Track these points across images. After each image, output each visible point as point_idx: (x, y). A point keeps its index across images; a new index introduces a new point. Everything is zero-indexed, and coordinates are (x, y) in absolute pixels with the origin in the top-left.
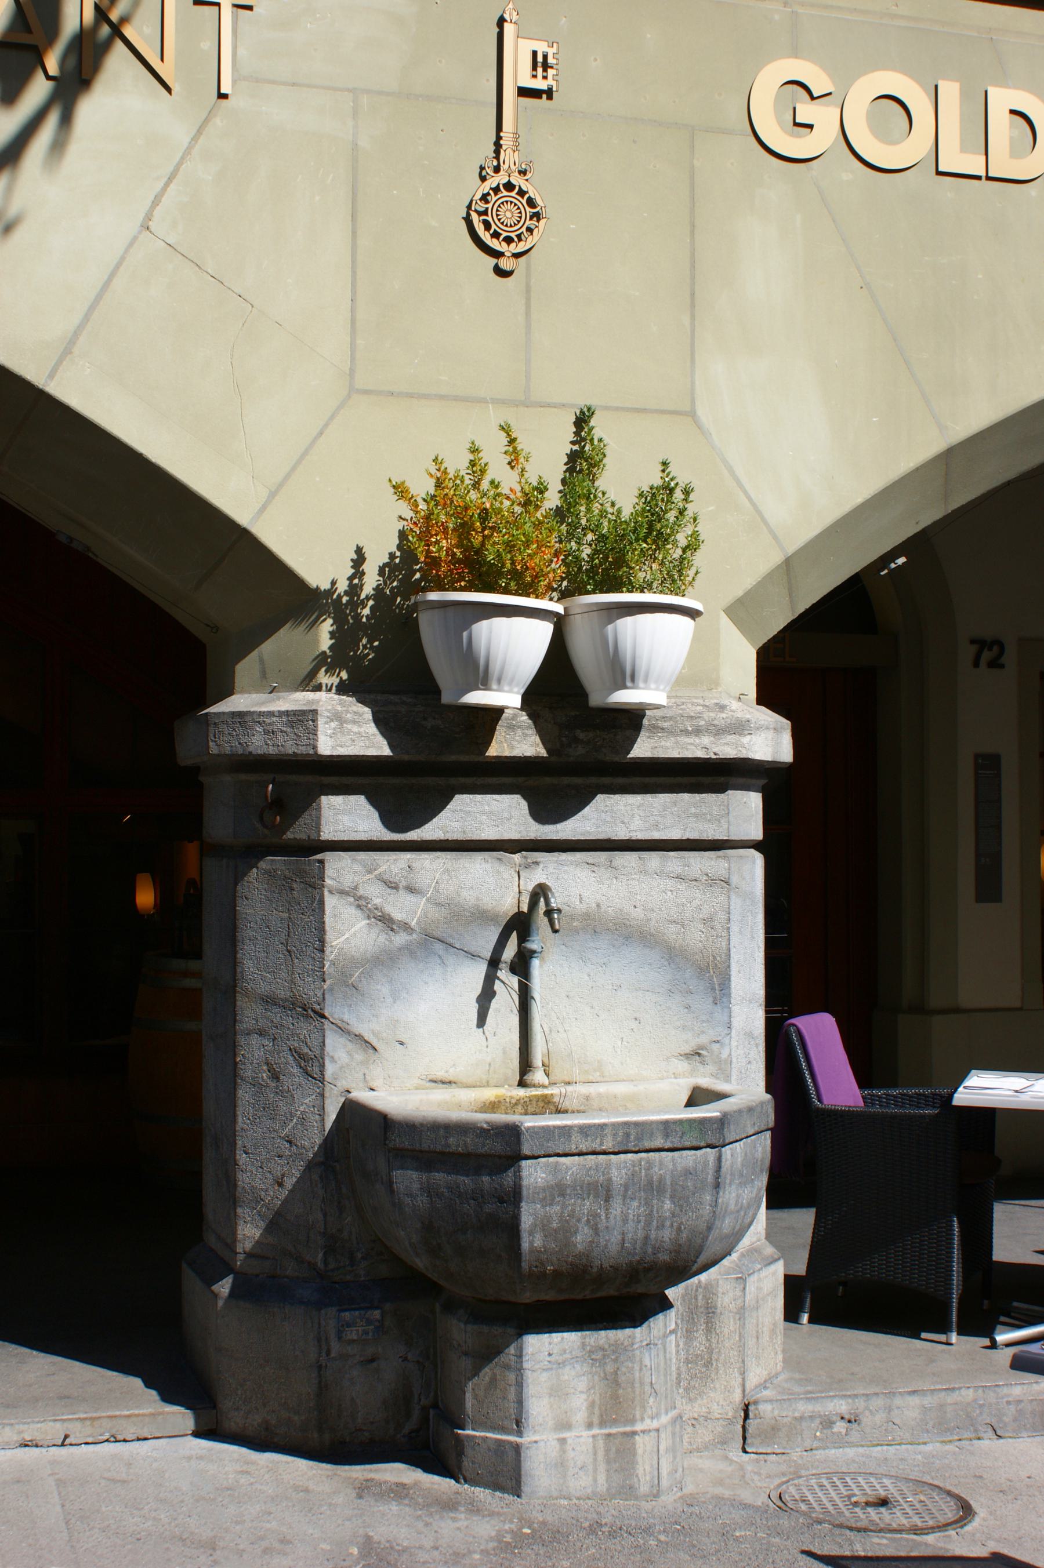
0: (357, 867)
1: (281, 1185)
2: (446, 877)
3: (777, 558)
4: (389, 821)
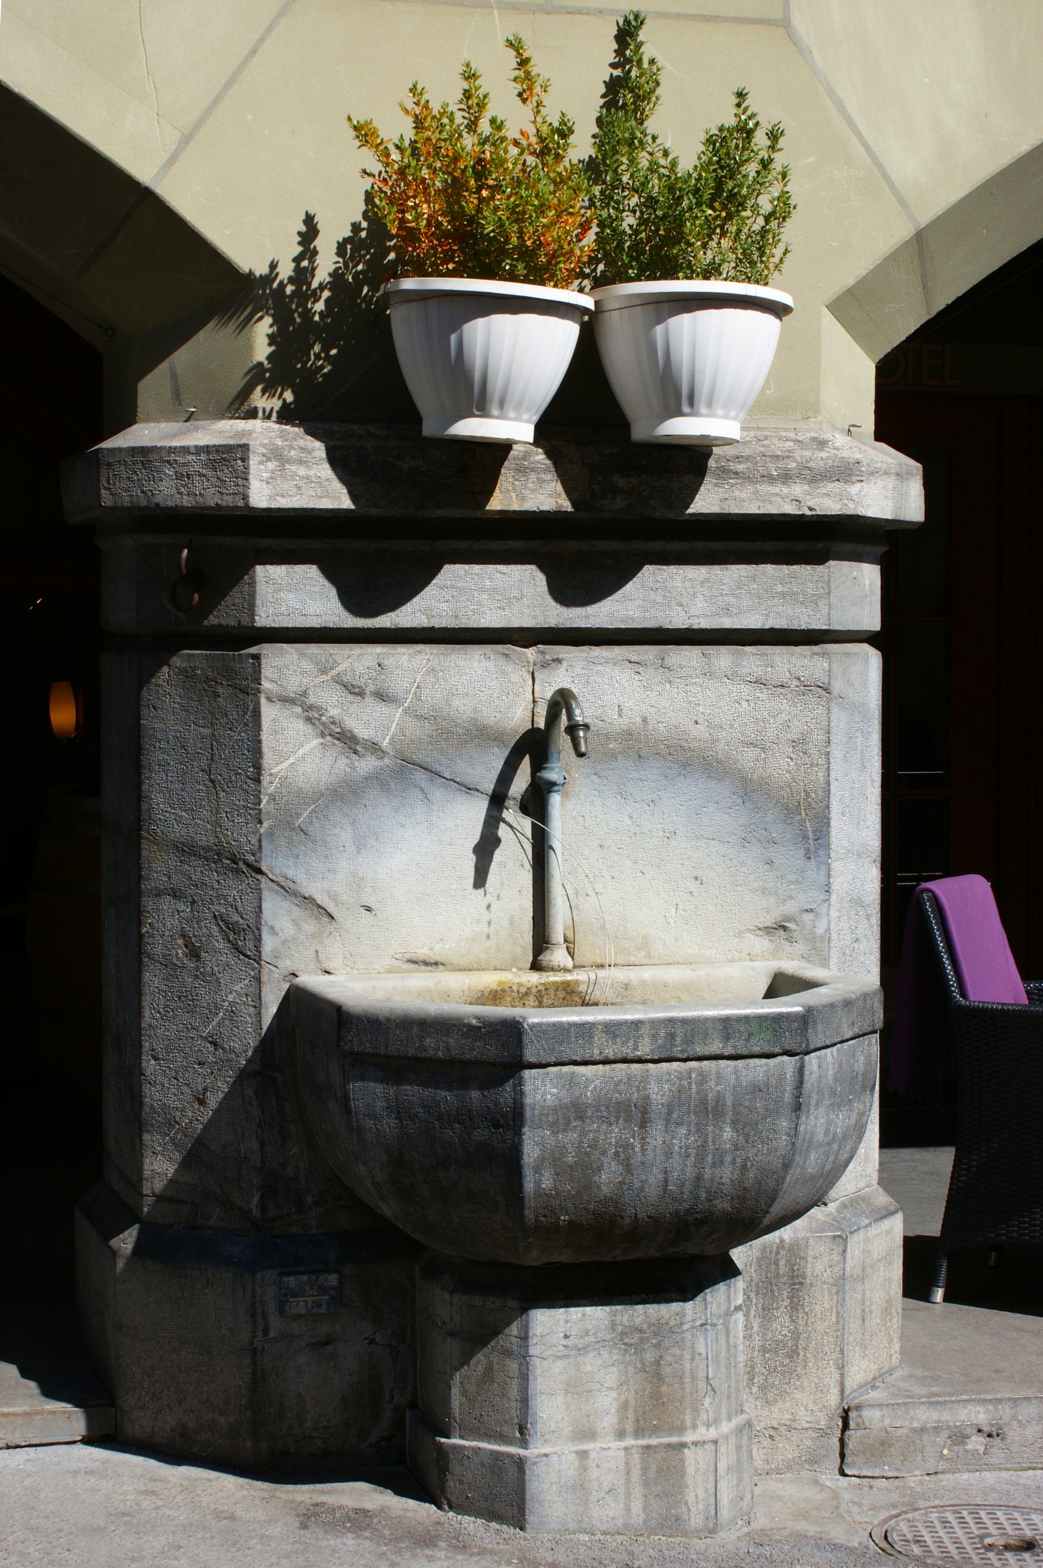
0: (306, 665)
1: (202, 1102)
2: (431, 679)
3: (904, 232)
4: (351, 601)
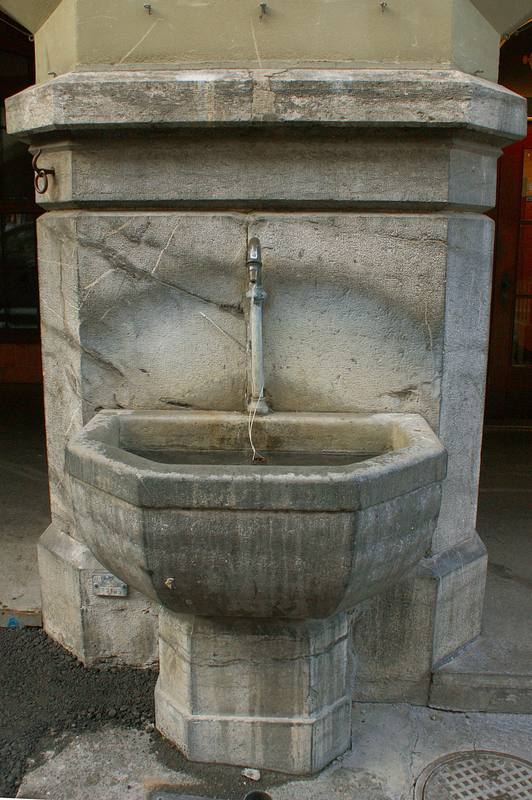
2: (181, 232)
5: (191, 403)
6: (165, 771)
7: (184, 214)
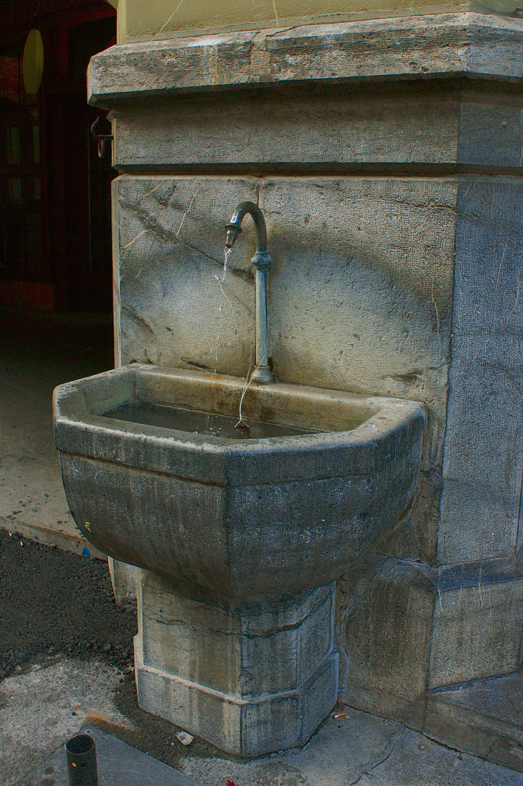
5: (207, 365)
6: (113, 711)
7: (203, 178)
